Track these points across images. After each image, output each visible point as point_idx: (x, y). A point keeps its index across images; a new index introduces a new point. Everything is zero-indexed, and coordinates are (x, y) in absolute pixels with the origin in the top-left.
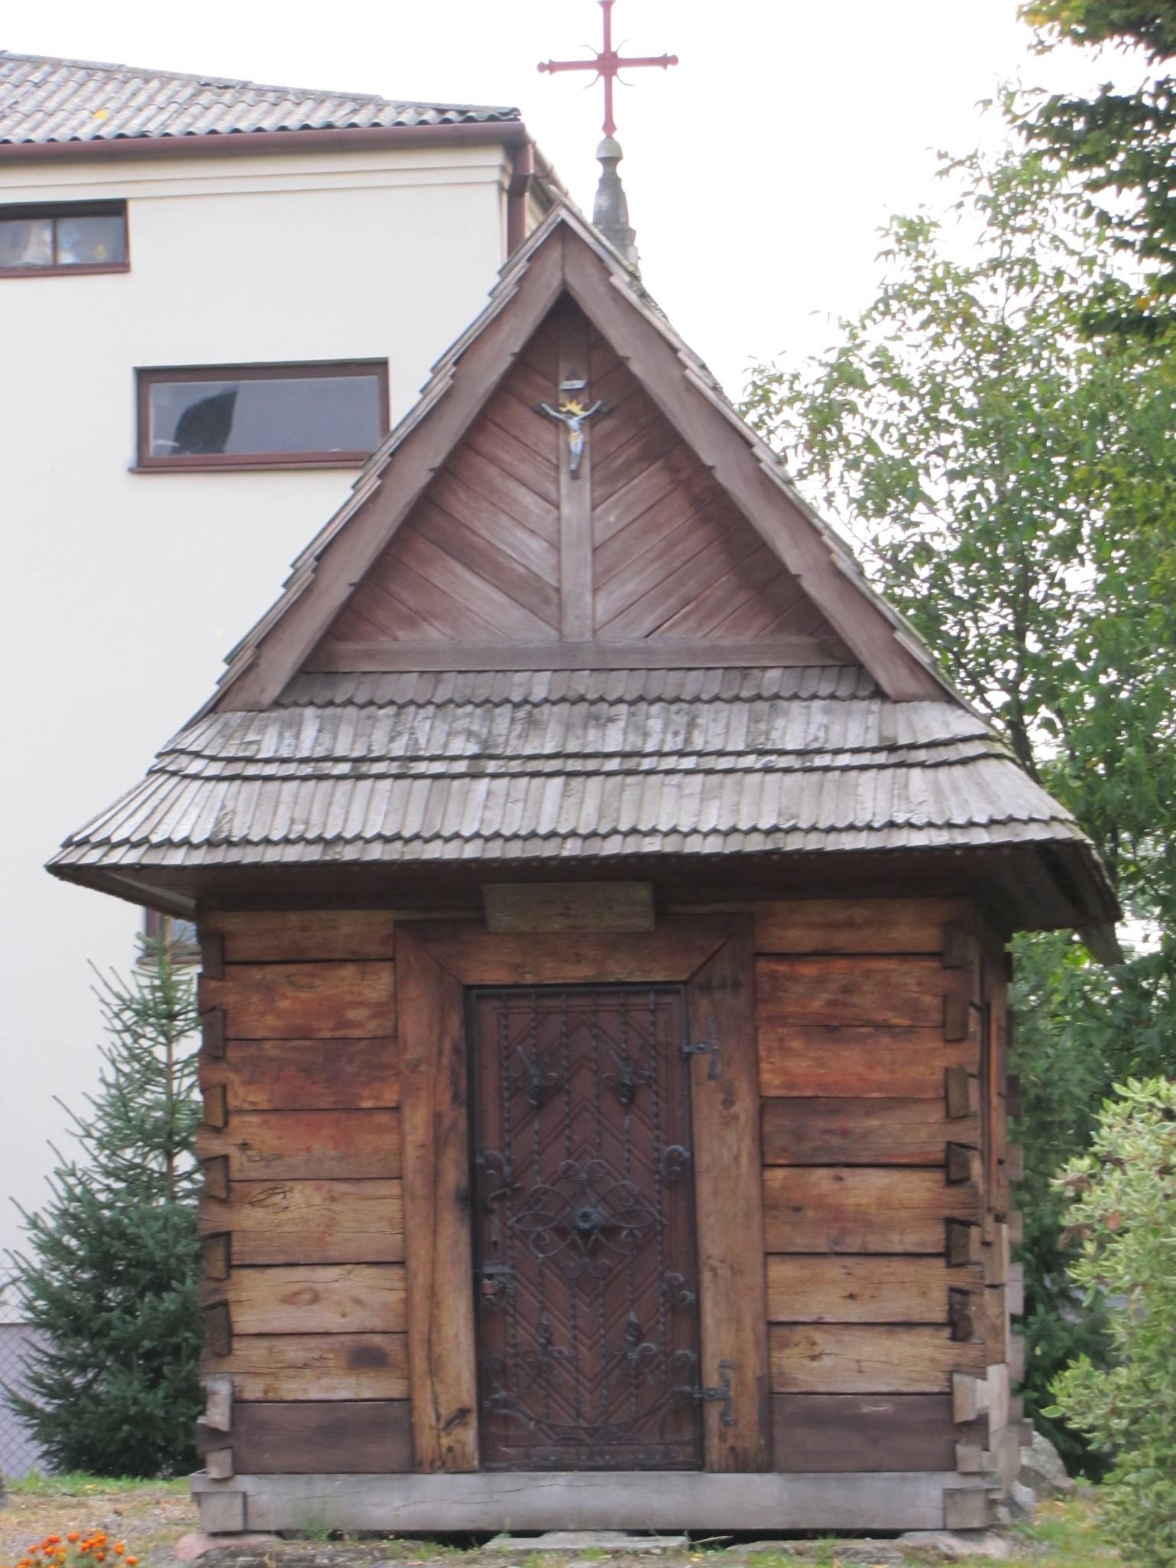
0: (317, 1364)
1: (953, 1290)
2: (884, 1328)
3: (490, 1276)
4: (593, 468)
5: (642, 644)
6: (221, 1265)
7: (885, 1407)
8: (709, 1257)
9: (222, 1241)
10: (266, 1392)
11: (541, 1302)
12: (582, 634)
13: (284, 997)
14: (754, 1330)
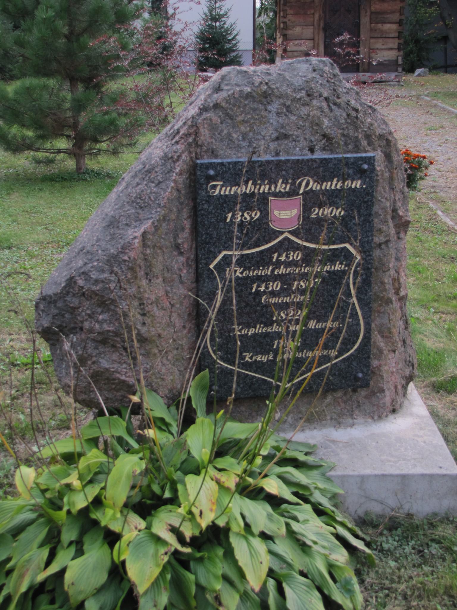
7: (387, 62)
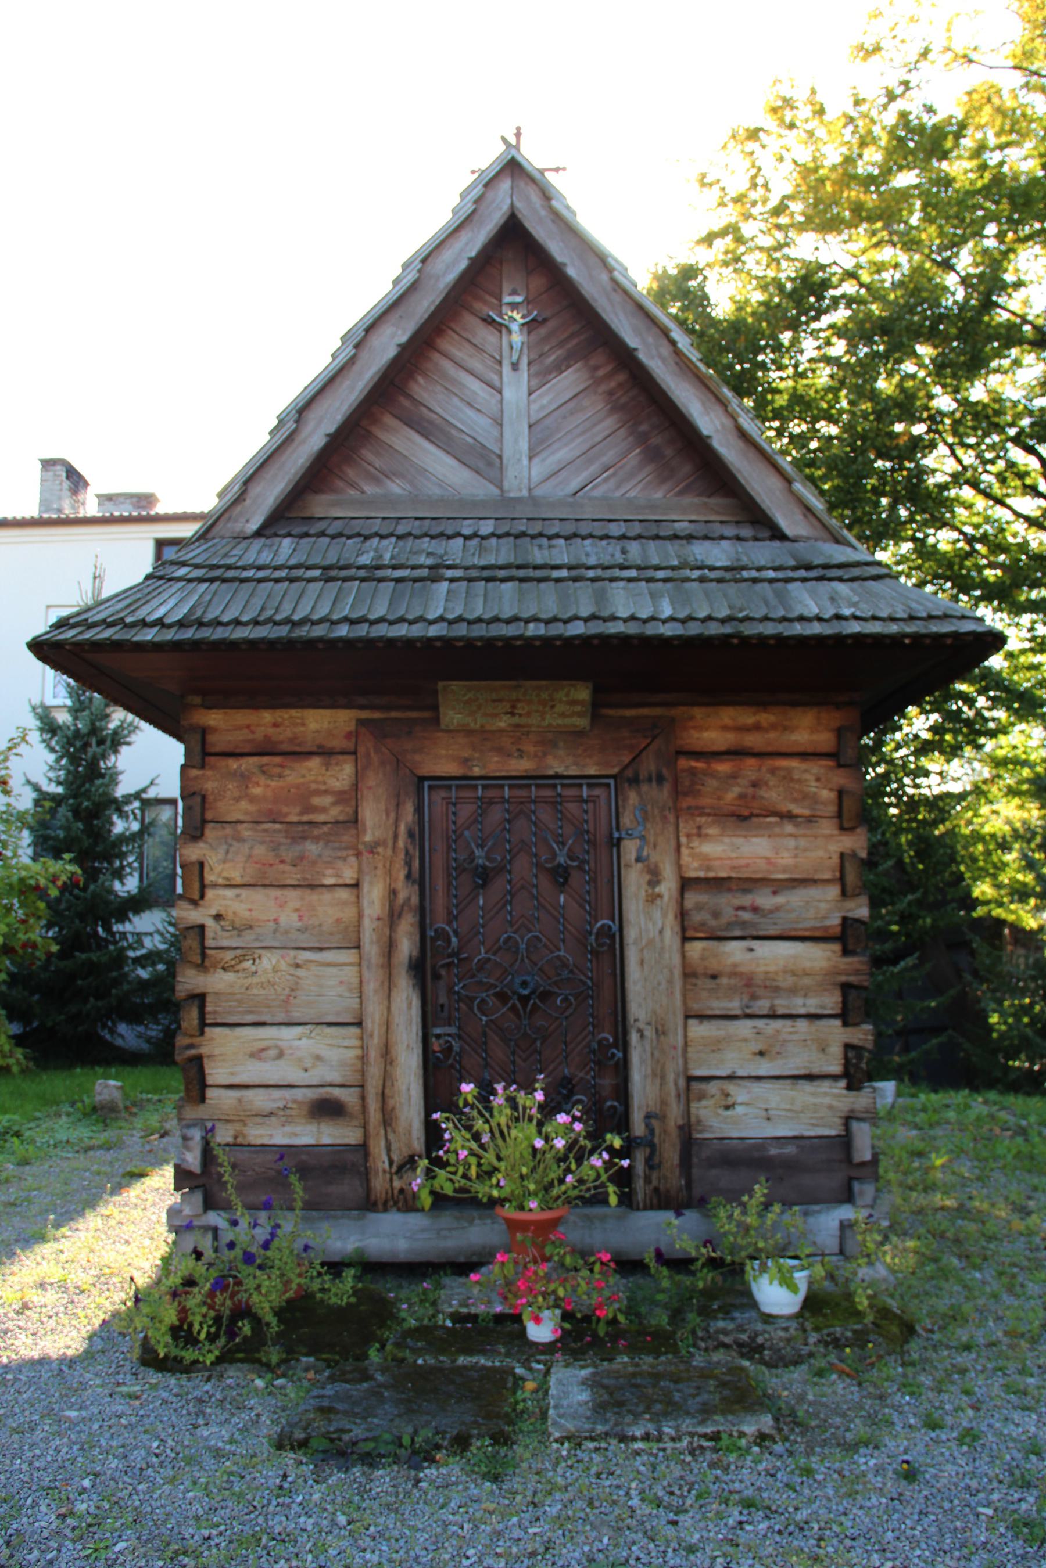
0: (281, 1113)
1: (848, 1047)
2: (788, 1081)
3: (438, 1036)
4: (529, 364)
5: (571, 500)
6: (196, 1022)
7: (790, 1150)
8: (636, 1020)
9: (196, 1002)
10: (236, 1137)
11: (485, 1059)
12: (520, 490)
13: (258, 784)
14: (676, 1084)
